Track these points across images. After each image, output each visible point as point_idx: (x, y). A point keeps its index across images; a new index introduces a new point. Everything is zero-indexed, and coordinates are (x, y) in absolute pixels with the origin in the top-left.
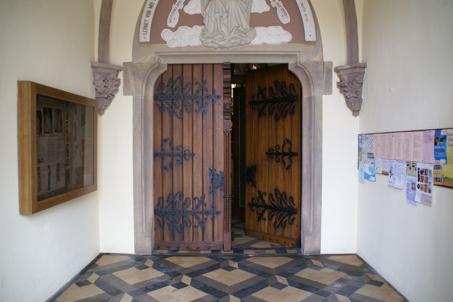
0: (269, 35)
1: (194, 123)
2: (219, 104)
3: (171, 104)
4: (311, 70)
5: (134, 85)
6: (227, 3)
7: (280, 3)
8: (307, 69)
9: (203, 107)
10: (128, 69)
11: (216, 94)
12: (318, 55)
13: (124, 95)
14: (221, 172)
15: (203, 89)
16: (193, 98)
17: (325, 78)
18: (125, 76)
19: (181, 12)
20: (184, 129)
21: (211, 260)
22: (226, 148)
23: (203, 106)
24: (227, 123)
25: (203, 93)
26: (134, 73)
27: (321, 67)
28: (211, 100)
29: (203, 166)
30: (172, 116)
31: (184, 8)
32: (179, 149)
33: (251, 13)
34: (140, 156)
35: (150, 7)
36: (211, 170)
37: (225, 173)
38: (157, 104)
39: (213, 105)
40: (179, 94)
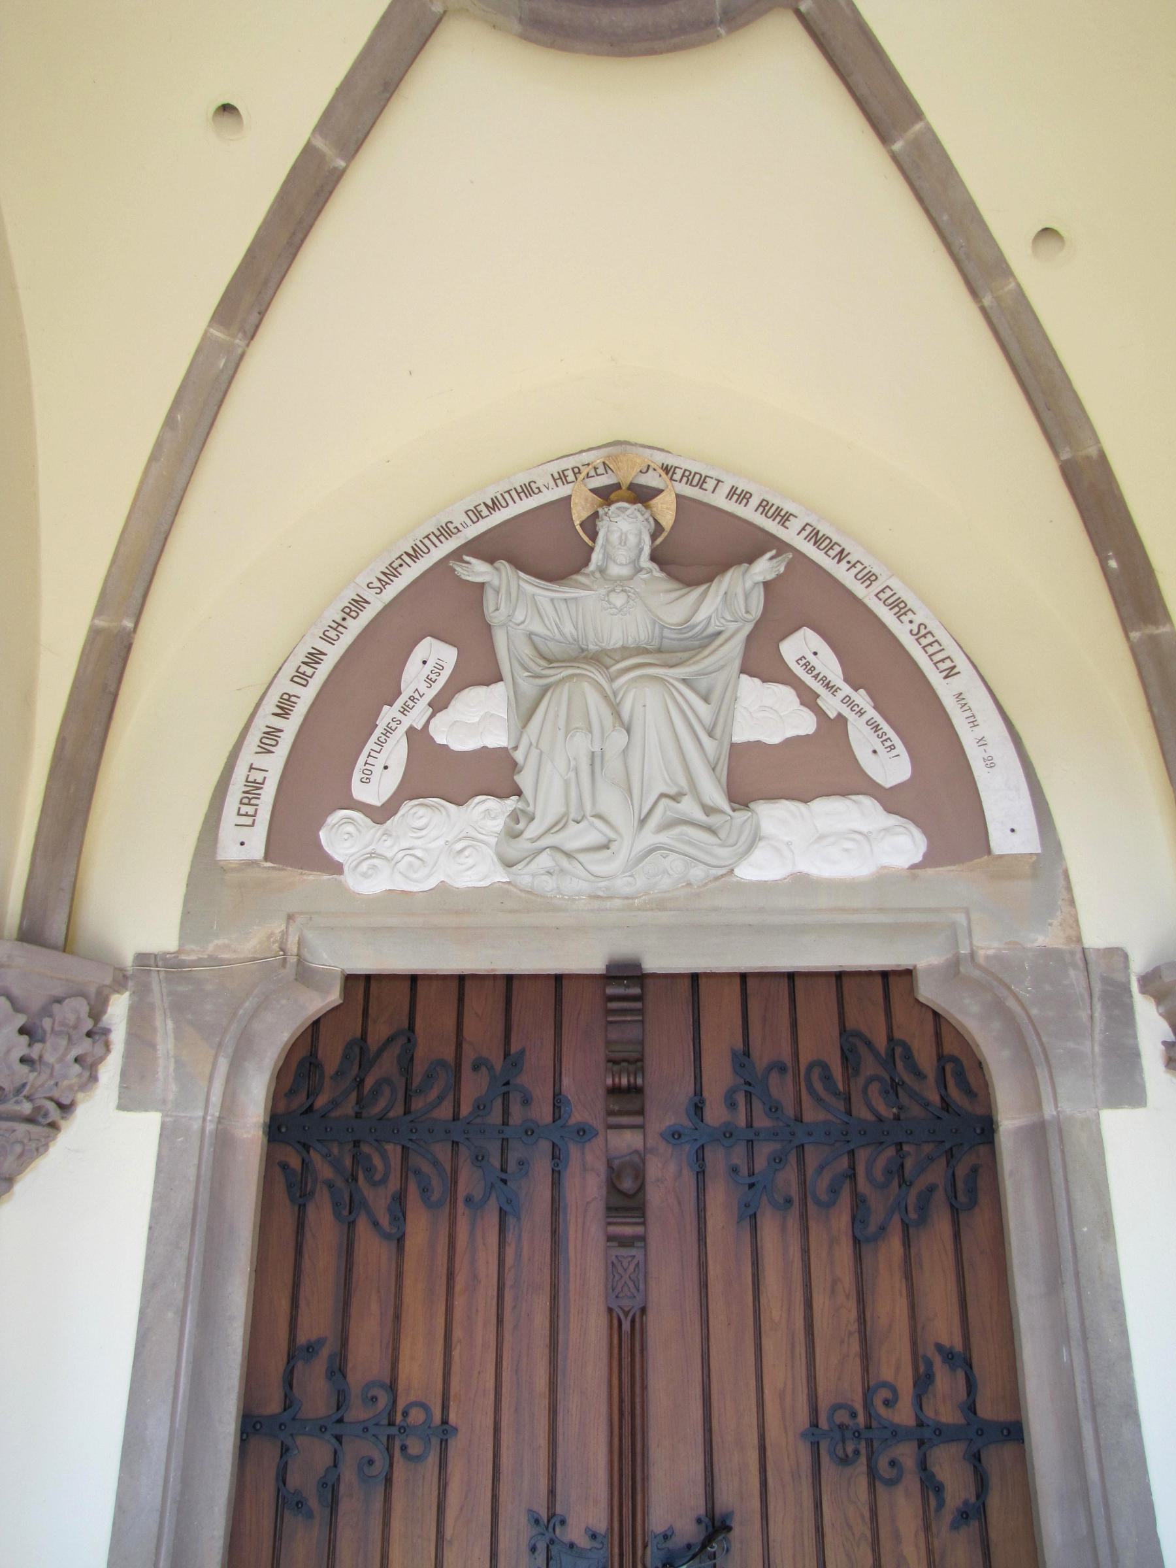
0: (822, 837)
1: (457, 1266)
2: (584, 1169)
3: (348, 1162)
4: (1028, 992)
5: (173, 1060)
6: (625, 693)
7: (862, 698)
8: (1009, 988)
9: (504, 1182)
10: (155, 987)
11: (572, 1121)
12: (1055, 922)
13: (121, 1107)
14: (594, 1536)
15: (505, 1096)
16: (456, 1139)
17: (1099, 1025)
18: (139, 1018)
19: (418, 738)
20: (408, 1282)
21: (733, 574)
22: (621, 1401)
23: (504, 1176)
24: (625, 1264)
25: (506, 1112)
26: (179, 1007)
27: (1075, 976)
28: (545, 1146)
29: (495, 1498)
30: (352, 1225)
31: (432, 722)
32: (374, 1399)
33: (733, 745)
34: (163, 1433)
35: (280, 711)
36: (537, 1522)
37: (616, 1543)
38: (279, 1164)
39: (556, 1175)
40: (391, 1114)
